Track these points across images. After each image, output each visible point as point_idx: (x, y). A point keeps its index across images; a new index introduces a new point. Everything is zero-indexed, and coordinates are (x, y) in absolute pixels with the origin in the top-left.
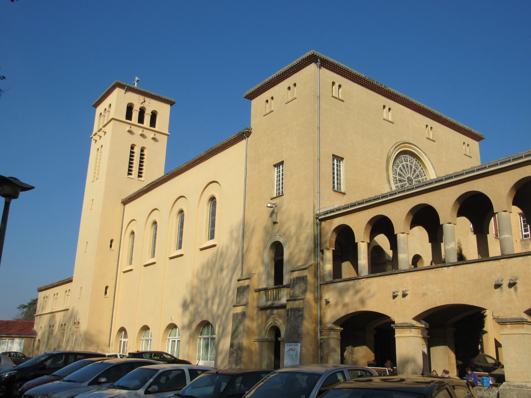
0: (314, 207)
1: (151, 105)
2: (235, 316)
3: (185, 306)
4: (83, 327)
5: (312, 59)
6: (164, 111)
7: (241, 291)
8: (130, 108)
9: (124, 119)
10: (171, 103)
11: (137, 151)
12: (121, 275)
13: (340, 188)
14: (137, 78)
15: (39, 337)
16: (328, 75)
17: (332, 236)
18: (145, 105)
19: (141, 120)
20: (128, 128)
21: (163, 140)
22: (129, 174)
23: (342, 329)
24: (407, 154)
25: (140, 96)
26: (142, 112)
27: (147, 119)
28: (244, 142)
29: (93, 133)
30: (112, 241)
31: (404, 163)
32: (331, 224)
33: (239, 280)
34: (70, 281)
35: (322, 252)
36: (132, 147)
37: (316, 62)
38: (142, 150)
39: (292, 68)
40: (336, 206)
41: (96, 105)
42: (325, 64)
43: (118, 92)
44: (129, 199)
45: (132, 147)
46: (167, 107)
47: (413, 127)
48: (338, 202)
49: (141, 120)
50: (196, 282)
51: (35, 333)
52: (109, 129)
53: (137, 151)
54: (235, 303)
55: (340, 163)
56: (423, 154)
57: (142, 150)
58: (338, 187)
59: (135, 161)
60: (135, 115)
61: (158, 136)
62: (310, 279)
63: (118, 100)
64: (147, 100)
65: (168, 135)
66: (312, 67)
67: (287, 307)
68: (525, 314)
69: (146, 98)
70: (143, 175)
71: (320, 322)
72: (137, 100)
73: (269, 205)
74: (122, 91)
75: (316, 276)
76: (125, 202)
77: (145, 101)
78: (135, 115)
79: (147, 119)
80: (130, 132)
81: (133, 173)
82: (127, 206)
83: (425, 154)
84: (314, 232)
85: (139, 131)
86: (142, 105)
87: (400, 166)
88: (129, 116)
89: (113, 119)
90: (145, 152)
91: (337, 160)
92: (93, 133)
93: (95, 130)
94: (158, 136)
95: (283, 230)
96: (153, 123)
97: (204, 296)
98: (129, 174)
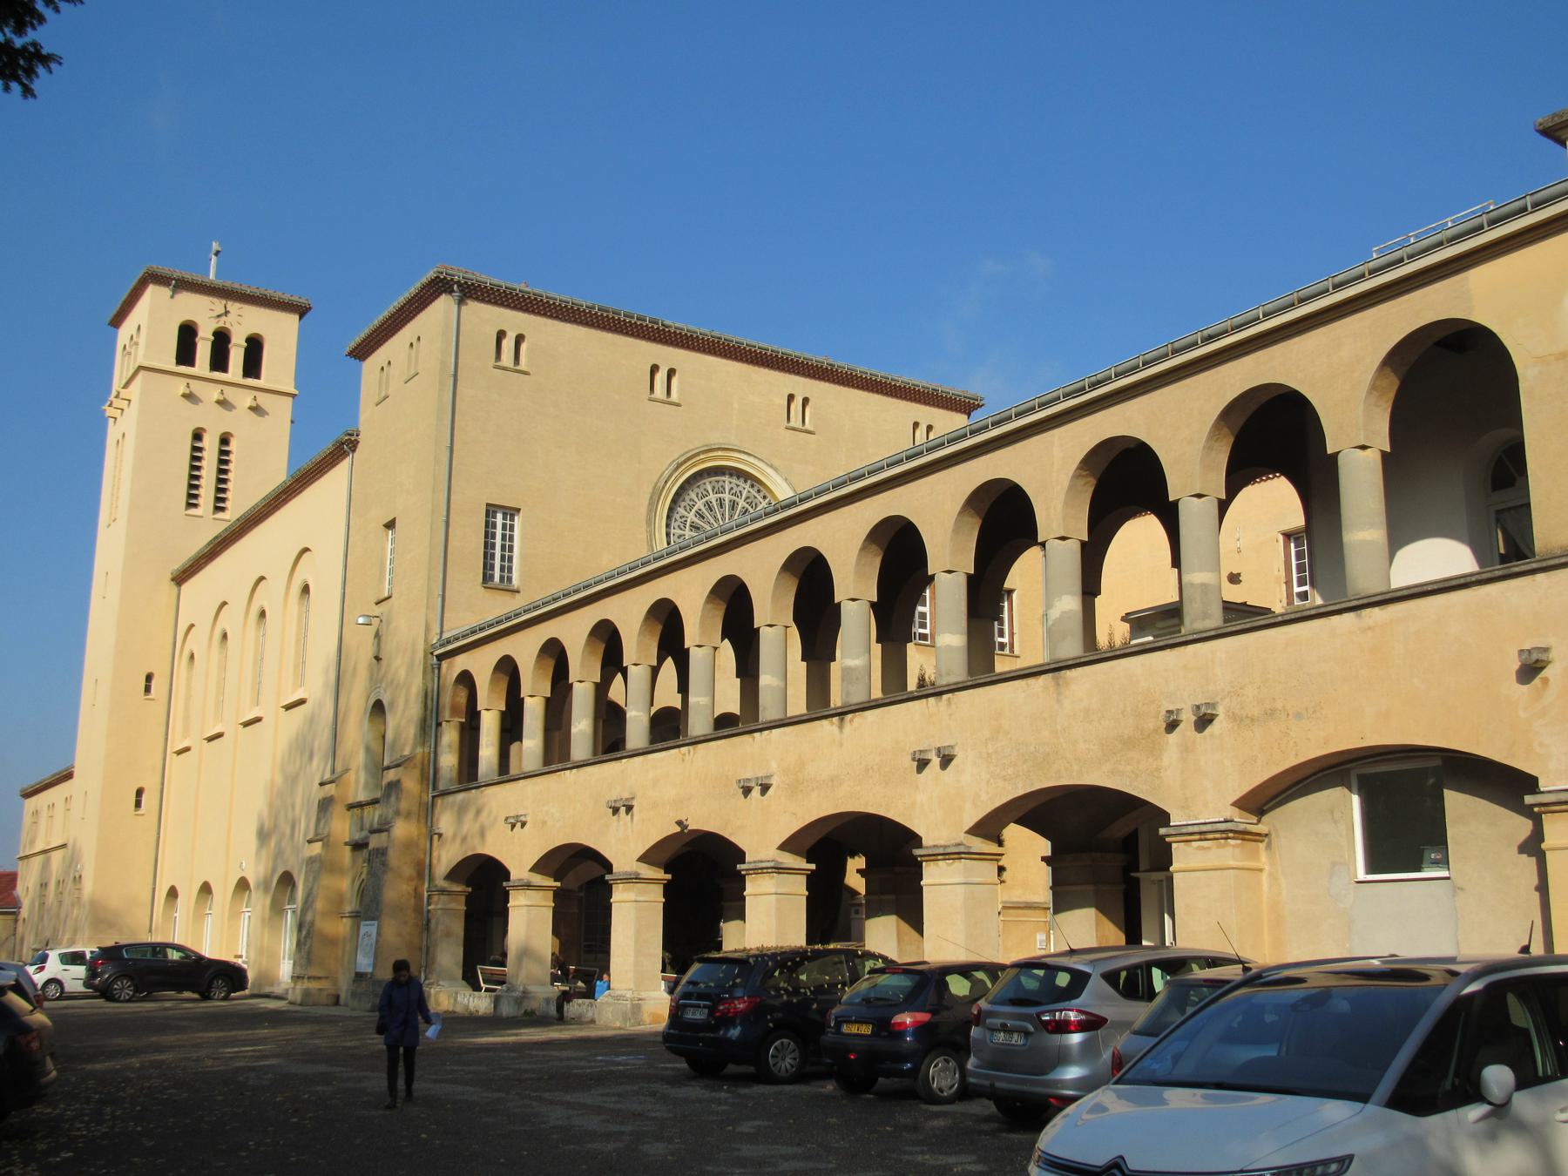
0: (428, 630)
1: (244, 321)
2: (311, 861)
3: (263, 836)
4: (88, 887)
5: (437, 287)
6: (281, 335)
7: (325, 805)
8: (187, 333)
9: (169, 362)
10: (302, 311)
11: (210, 445)
12: (172, 759)
13: (510, 579)
14: (215, 246)
15: (24, 913)
16: (484, 318)
17: (455, 695)
18: (228, 322)
19: (219, 360)
20: (180, 386)
21: (281, 410)
22: (190, 505)
23: (669, 876)
24: (723, 474)
25: (215, 300)
26: (221, 340)
27: (236, 357)
28: (345, 465)
29: (114, 393)
30: (149, 678)
31: (712, 498)
32: (450, 667)
33: (322, 784)
34: (68, 776)
35: (439, 725)
36: (198, 436)
37: (451, 292)
38: (225, 440)
39: (410, 302)
40: (490, 617)
41: (117, 320)
42: (471, 291)
43: (154, 295)
44: (184, 572)
45: (198, 436)
46: (292, 320)
47: (732, 406)
48: (495, 607)
49: (219, 360)
50: (279, 779)
51: (16, 904)
52: (135, 390)
53: (210, 445)
54: (311, 836)
55: (512, 519)
56: (769, 471)
57: (225, 440)
58: (502, 578)
59: (206, 465)
60: (203, 351)
61: (265, 400)
62: (411, 783)
63: (154, 318)
64: (234, 307)
65: (294, 396)
66: (443, 305)
67: (371, 846)
68: (786, 854)
69: (230, 303)
70: (228, 504)
71: (423, 870)
72: (205, 313)
73: (361, 620)
74: (165, 292)
75: (424, 777)
76: (181, 578)
77: (227, 313)
78: (203, 351)
79: (236, 357)
80: (189, 396)
81: (201, 501)
82: (186, 587)
83: (776, 470)
84: (425, 684)
85: (214, 393)
86: (221, 324)
87: (700, 504)
88: (186, 354)
89: (141, 368)
90: (233, 446)
91: (505, 515)
92: (114, 393)
93: (117, 384)
94: (265, 400)
95: (390, 676)
96: (252, 365)
97: (290, 814)
98: (190, 505)
